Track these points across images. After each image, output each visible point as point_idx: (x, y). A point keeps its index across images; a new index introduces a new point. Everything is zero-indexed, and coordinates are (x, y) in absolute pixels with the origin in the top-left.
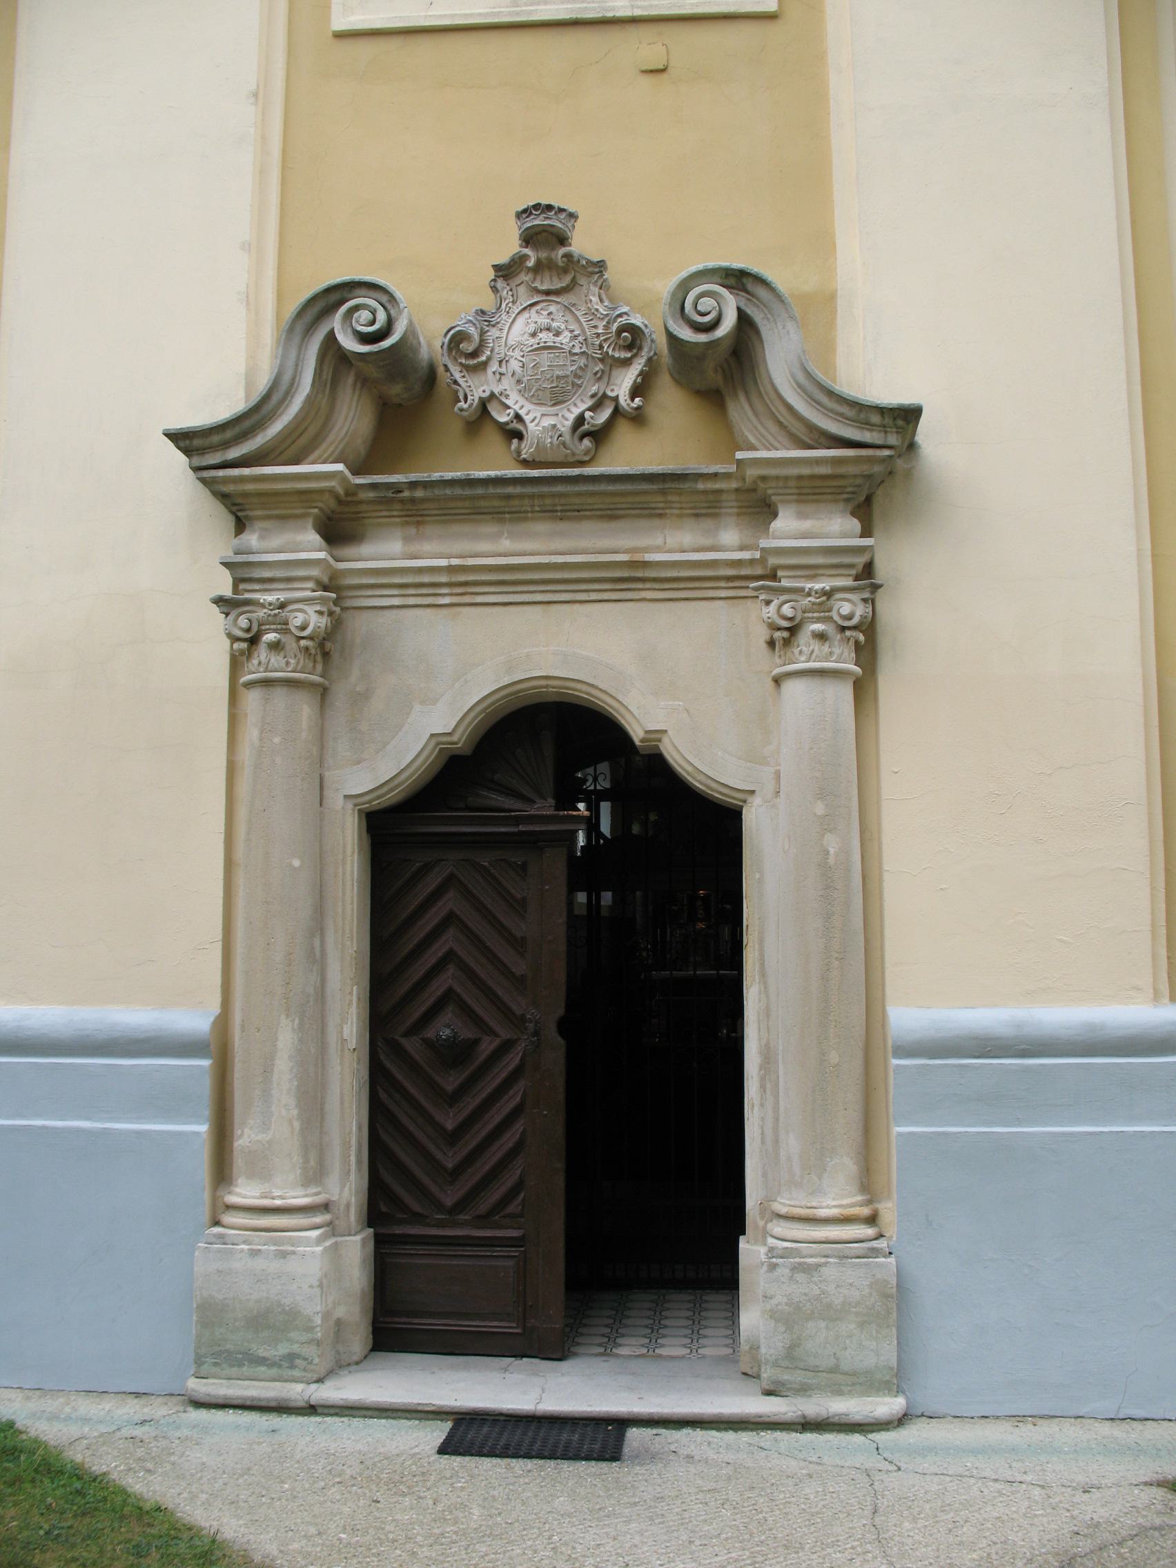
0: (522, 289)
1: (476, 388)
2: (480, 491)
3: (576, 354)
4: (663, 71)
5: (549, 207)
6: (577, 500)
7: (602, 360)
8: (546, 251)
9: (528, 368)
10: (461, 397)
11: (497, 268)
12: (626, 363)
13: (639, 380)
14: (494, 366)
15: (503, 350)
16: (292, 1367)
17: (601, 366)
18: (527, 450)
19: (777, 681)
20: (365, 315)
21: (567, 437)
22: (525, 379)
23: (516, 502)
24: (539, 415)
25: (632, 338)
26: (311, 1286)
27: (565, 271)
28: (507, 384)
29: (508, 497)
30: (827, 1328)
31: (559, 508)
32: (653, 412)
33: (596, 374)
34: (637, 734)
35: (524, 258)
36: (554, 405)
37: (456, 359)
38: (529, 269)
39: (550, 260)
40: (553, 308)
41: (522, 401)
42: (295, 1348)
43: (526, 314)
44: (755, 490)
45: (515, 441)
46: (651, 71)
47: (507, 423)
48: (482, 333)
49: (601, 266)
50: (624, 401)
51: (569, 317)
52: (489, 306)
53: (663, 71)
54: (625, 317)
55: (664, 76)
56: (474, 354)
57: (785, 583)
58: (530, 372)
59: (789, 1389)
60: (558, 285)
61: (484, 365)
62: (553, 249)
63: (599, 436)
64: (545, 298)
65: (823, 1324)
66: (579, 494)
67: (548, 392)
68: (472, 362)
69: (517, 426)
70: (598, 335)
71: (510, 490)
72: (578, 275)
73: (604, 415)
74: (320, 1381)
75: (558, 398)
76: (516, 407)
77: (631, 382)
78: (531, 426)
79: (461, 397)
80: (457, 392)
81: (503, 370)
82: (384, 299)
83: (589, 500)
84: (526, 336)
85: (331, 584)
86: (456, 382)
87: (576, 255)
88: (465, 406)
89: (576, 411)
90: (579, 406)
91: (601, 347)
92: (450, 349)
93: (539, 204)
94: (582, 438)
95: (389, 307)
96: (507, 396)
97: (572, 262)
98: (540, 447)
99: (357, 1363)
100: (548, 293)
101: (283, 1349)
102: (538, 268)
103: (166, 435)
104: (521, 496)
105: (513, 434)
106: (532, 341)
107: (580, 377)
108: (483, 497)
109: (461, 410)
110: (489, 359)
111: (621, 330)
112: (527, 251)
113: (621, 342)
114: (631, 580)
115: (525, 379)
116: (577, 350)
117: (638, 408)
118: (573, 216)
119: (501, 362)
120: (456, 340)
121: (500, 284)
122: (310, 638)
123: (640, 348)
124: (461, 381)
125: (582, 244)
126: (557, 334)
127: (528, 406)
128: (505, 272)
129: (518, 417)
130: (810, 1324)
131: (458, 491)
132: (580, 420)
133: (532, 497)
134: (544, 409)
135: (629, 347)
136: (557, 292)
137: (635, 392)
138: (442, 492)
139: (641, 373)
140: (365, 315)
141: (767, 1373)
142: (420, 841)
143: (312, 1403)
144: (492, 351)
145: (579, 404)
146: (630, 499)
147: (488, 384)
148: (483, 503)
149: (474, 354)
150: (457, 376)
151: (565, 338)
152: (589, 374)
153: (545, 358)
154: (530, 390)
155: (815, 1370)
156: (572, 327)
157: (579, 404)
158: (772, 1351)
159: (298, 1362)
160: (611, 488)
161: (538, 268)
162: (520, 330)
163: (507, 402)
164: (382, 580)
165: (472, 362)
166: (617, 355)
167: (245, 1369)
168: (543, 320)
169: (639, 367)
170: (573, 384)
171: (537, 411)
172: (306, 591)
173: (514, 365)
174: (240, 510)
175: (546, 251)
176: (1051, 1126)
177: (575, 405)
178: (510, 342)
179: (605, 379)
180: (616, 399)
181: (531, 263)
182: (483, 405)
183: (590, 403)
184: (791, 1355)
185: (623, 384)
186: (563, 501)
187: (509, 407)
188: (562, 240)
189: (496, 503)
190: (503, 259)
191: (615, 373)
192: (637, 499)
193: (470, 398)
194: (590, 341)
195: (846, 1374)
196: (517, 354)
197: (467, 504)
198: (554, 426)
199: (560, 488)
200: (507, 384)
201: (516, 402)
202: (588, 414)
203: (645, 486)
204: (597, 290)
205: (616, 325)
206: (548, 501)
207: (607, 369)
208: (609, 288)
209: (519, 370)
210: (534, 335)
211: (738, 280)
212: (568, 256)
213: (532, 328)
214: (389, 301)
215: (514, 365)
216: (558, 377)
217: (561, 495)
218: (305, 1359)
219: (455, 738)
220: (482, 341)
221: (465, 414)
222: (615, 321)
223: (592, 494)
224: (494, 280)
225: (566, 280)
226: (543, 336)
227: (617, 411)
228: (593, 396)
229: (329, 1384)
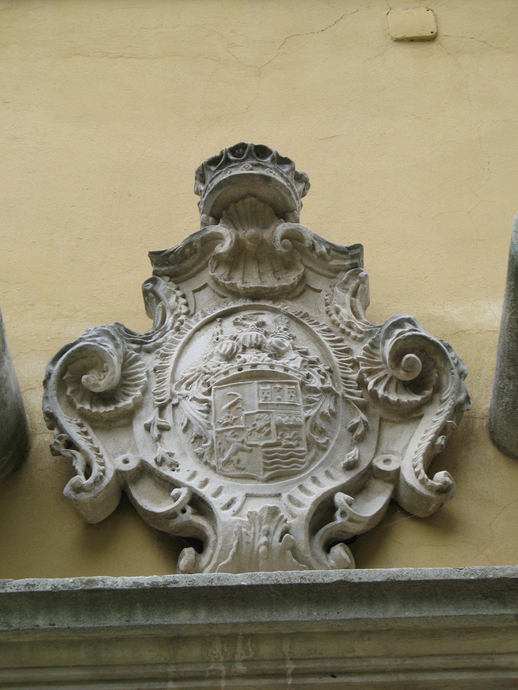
0: (205, 296)
1: (113, 456)
2: (114, 620)
3: (314, 390)
4: (431, 39)
5: (262, 151)
6: (331, 648)
7: (364, 408)
8: (250, 224)
10: (79, 466)
11: (159, 258)
12: (412, 415)
13: (440, 440)
14: (149, 415)
15: (168, 388)
17: (362, 416)
21: (300, 536)
22: (212, 433)
23: (194, 652)
24: (240, 496)
25: (423, 365)
27: (287, 265)
28: (174, 444)
29: (176, 639)
31: (291, 666)
32: (462, 506)
33: (353, 430)
36: (269, 480)
37: (71, 404)
38: (220, 260)
39: (260, 243)
40: (267, 318)
41: (203, 473)
43: (214, 329)
46: (412, 40)
47: (172, 515)
48: (127, 363)
49: (354, 253)
50: (409, 476)
52: (141, 325)
53: (431, 39)
55: (433, 47)
56: (108, 397)
58: (222, 419)
60: (270, 282)
61: (128, 417)
62: (265, 227)
63: (364, 544)
64: (249, 303)
66: (336, 633)
67: (259, 454)
70: (355, 364)
71: (183, 618)
72: (310, 275)
73: (374, 505)
75: (281, 465)
76: (195, 484)
77: (426, 444)
78: (224, 516)
79: (79, 466)
80: (69, 461)
81: (168, 419)
83: (361, 648)
84: (215, 360)
86: (70, 444)
87: (308, 236)
89: (318, 492)
91: (362, 384)
92: (62, 385)
93: (243, 146)
94: (328, 547)
96: (174, 466)
97: (302, 250)
98: (243, 559)
100: (256, 295)
102: (237, 258)
104: (205, 638)
105: (179, 539)
106: (225, 366)
107: (322, 432)
108: (119, 639)
109: (78, 489)
110: (138, 406)
111: (397, 355)
112: (220, 229)
113: (402, 375)
115: (212, 433)
116: (315, 383)
117: (443, 490)
119: (162, 408)
120: (74, 366)
121: (164, 286)
123: (438, 389)
124: (79, 439)
125: (318, 218)
126: (277, 354)
127: (216, 481)
128: (174, 265)
129: (198, 503)
131: (64, 620)
132: (325, 509)
133: (230, 639)
134: (250, 486)
135: (414, 386)
136: (275, 295)
137: (433, 462)
138: (27, 624)
139: (443, 430)
142: (169, 427)
144: (145, 391)
145: (322, 478)
146: (451, 645)
147: (135, 450)
148: (120, 654)
150: (73, 430)
151: (292, 361)
152: (340, 429)
153: (253, 394)
154: (222, 452)
156: (305, 348)
157: (322, 478)
160: (411, 613)
161: (237, 258)
162: (198, 351)
163: (175, 475)
166: (393, 397)
168: (249, 333)
169: (440, 419)
171: (236, 490)
173: (191, 410)
175: (250, 224)
177: (315, 480)
178: (178, 378)
179: (372, 440)
181: (223, 248)
182: (123, 485)
183: (343, 479)
185: (407, 452)
186: (300, 649)
187: (175, 484)
188: (284, 212)
189: (149, 654)
190: (173, 241)
191: (388, 433)
192: (471, 644)
194: (339, 372)
196: (197, 390)
197: (82, 655)
198: (274, 512)
199: (295, 615)
201: (190, 473)
202: (341, 498)
203: (489, 611)
204: (347, 297)
205: (389, 344)
206: (266, 650)
207: (374, 425)
208: (366, 292)
210: (229, 357)
212: (295, 238)
213: (226, 346)
215: (191, 410)
216: (279, 426)
217: (298, 634)
220: (124, 377)
221: (84, 496)
222: (388, 335)
223: (367, 632)
224: (153, 280)
225: (290, 279)
226: (250, 356)
227: (394, 506)
228: (350, 467)
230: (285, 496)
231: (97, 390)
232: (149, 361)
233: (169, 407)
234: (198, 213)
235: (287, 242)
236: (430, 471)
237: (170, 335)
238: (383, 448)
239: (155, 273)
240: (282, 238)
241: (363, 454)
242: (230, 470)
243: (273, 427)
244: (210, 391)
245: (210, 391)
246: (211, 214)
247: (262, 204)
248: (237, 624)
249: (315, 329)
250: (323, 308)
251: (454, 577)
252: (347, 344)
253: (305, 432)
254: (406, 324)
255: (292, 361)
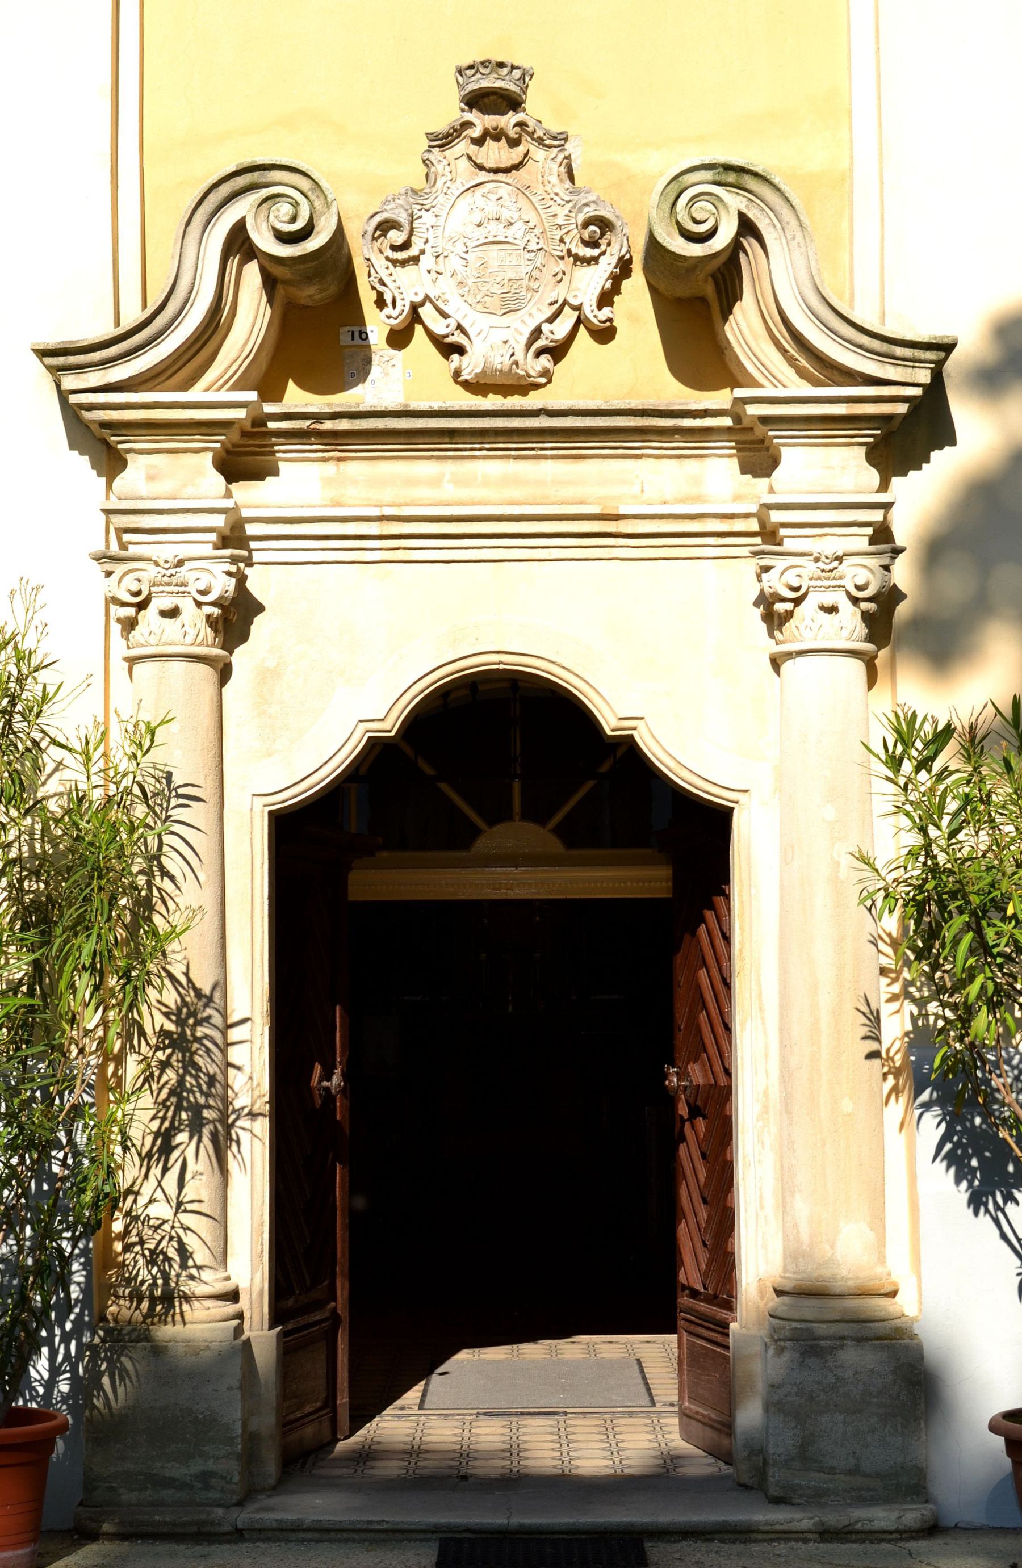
1: (408, 285)
9: (472, 274)
10: (389, 301)
16: (207, 1487)
18: (471, 365)
19: (776, 663)
20: (285, 209)
26: (230, 1389)
30: (845, 1422)
34: (609, 723)
35: (467, 125)
42: (211, 1465)
44: (751, 429)
45: (455, 357)
49: (561, 139)
50: (590, 310)
51: (523, 202)
52: (420, 184)
54: (593, 206)
56: (406, 246)
57: (788, 545)
59: (801, 1496)
61: (415, 260)
63: (558, 352)
65: (839, 1417)
68: (400, 256)
69: (458, 338)
74: (240, 1504)
79: (389, 301)
82: (304, 184)
84: (471, 227)
85: (234, 537)
88: (395, 313)
90: (536, 313)
93: (489, 61)
94: (538, 354)
95: (312, 197)
99: (274, 1488)
101: (196, 1467)
103: (33, 350)
111: (586, 224)
114: (604, 530)
116: (533, 246)
118: (526, 75)
122: (213, 604)
130: (825, 1419)
135: (594, 244)
140: (285, 209)
141: (775, 1475)
143: (240, 1526)
149: (406, 246)
151: (517, 232)
152: (547, 276)
155: (832, 1471)
158: (780, 1450)
159: (213, 1481)
164: (296, 529)
165: (400, 256)
167: (149, 1492)
170: (528, 289)
172: (204, 546)
174: (101, 443)
176: (689, 791)
180: (578, 308)
184: (805, 1456)
190: (441, 125)
193: (399, 303)
195: (866, 1475)
200: (445, 290)
209: (460, 269)
211: (733, 175)
213: (477, 217)
214: (312, 190)
215: (454, 263)
218: (222, 1478)
219: (386, 725)
222: (580, 211)
229: (251, 1507)
230: (512, 328)
231: (398, 244)
232: (428, 218)
233: (442, 257)
234: (457, 102)
235: (517, 129)
236: (600, 307)
237: (442, 198)
238: (573, 286)
239: (430, 146)
240: (514, 126)
241: (561, 293)
242: (479, 307)
243: (506, 281)
244: (467, 252)
245: (467, 252)
246: (466, 104)
247: (500, 100)
248: (372, 1522)
249: (534, 199)
250: (540, 179)
251: (603, 408)
252: (556, 209)
253: (525, 283)
254: (592, 205)
255: (517, 232)
